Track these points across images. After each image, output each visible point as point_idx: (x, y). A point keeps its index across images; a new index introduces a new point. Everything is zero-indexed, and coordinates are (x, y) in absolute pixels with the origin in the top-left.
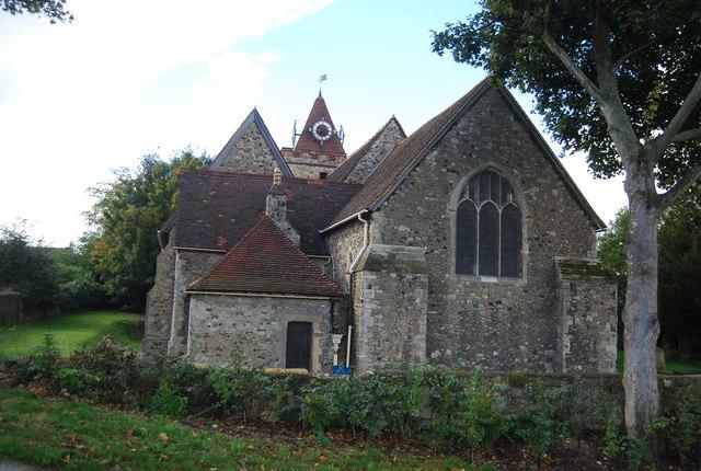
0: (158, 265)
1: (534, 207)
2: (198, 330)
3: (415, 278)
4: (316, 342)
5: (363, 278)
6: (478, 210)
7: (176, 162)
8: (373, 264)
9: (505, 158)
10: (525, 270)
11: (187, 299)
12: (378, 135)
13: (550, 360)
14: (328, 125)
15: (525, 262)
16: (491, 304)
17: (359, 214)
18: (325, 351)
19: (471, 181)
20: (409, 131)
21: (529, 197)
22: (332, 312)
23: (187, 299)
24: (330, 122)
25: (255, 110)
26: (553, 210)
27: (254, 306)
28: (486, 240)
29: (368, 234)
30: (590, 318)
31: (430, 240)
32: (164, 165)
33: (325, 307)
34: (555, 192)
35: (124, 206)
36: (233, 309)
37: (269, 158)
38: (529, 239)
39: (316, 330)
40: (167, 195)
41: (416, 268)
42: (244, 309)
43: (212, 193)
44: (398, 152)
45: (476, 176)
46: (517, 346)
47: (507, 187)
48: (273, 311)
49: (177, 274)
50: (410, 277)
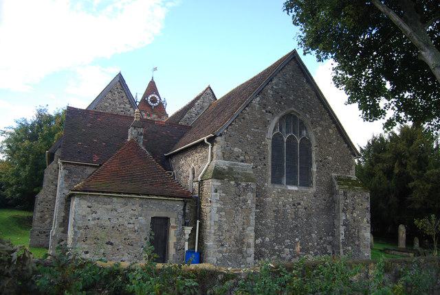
0: (45, 175)
1: (319, 140)
2: (80, 223)
3: (247, 185)
4: (172, 232)
5: (211, 184)
6: (285, 140)
7: (58, 115)
8: (218, 174)
9: (301, 107)
10: (314, 182)
11: (69, 199)
12: (198, 98)
13: (330, 243)
14: (157, 97)
15: (314, 176)
16: (294, 205)
17: (205, 138)
18: (179, 240)
19: (280, 120)
20: (219, 95)
21: (316, 133)
22: (184, 210)
23: (69, 199)
24: (159, 96)
25: (120, 74)
26: (330, 143)
27: (126, 204)
28: (290, 161)
29: (212, 153)
30: (355, 215)
31: (255, 159)
32: (50, 116)
33: (179, 206)
34: (331, 131)
35: (21, 140)
36: (108, 207)
37: (128, 106)
38: (317, 161)
39: (172, 223)
40: (51, 135)
41: (248, 178)
42: (118, 207)
43: (89, 125)
44: (211, 113)
45: (283, 117)
46: (310, 234)
47: (303, 126)
48: (140, 209)
49: (60, 182)
50: (244, 184)
